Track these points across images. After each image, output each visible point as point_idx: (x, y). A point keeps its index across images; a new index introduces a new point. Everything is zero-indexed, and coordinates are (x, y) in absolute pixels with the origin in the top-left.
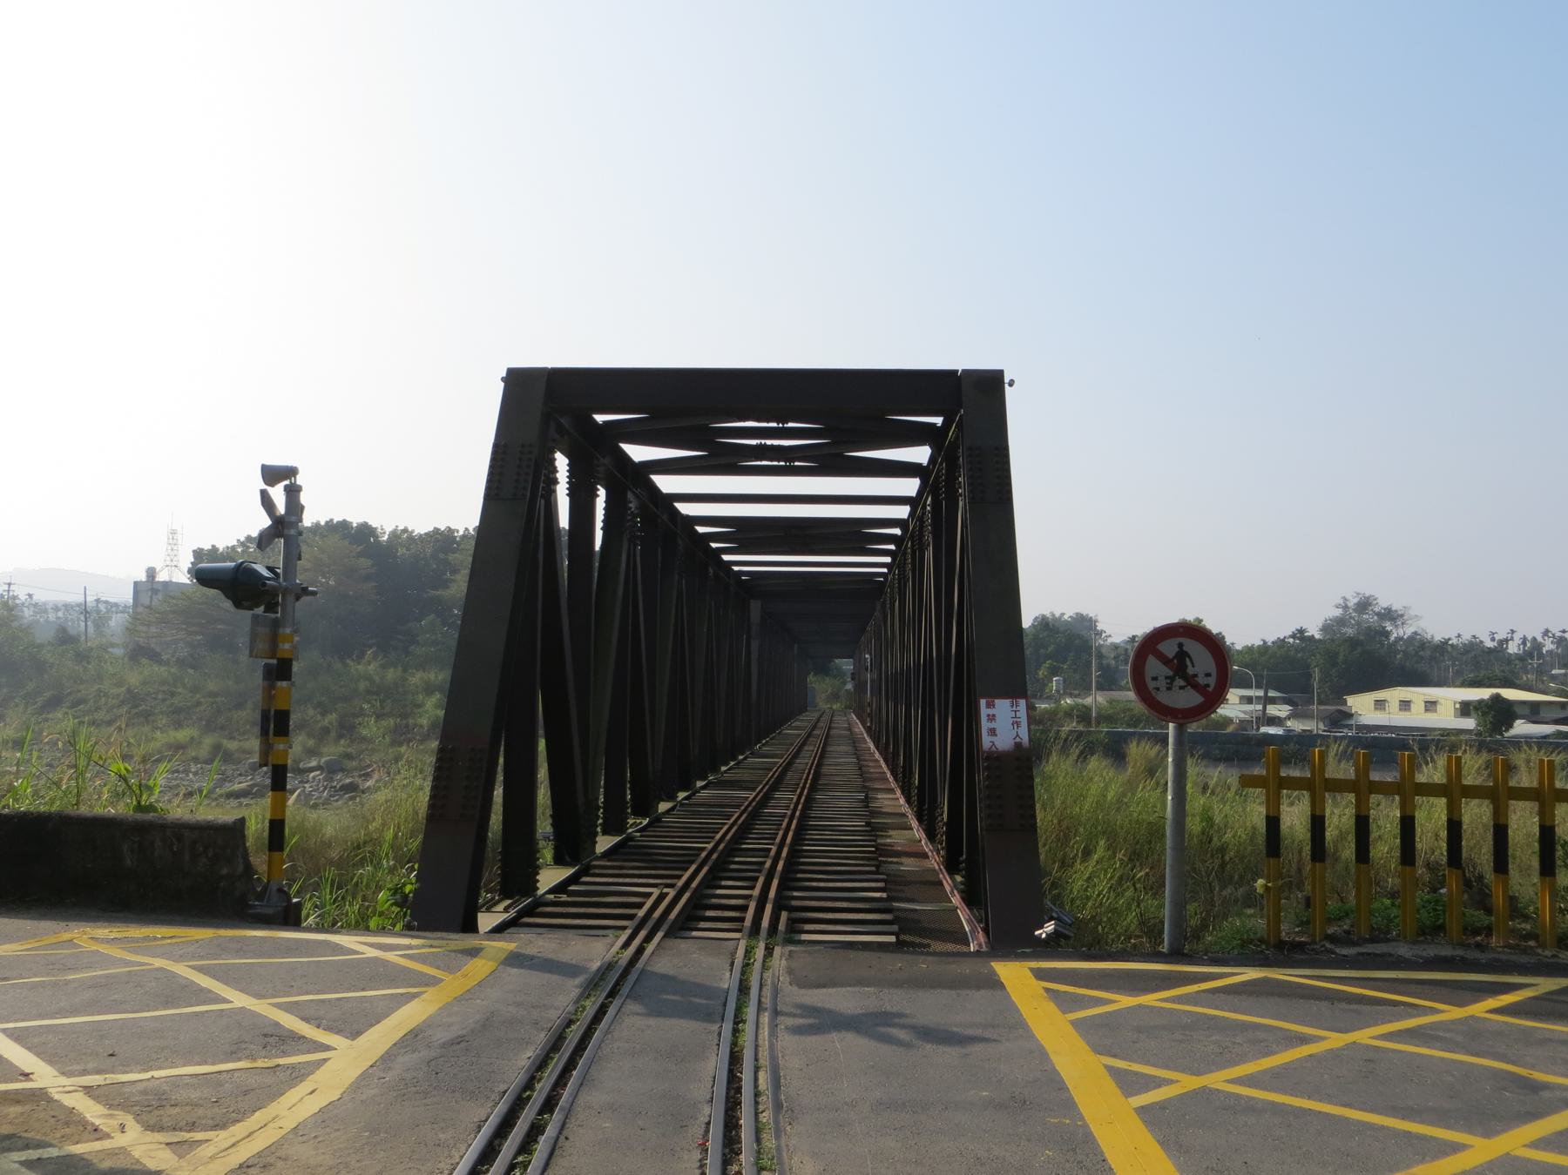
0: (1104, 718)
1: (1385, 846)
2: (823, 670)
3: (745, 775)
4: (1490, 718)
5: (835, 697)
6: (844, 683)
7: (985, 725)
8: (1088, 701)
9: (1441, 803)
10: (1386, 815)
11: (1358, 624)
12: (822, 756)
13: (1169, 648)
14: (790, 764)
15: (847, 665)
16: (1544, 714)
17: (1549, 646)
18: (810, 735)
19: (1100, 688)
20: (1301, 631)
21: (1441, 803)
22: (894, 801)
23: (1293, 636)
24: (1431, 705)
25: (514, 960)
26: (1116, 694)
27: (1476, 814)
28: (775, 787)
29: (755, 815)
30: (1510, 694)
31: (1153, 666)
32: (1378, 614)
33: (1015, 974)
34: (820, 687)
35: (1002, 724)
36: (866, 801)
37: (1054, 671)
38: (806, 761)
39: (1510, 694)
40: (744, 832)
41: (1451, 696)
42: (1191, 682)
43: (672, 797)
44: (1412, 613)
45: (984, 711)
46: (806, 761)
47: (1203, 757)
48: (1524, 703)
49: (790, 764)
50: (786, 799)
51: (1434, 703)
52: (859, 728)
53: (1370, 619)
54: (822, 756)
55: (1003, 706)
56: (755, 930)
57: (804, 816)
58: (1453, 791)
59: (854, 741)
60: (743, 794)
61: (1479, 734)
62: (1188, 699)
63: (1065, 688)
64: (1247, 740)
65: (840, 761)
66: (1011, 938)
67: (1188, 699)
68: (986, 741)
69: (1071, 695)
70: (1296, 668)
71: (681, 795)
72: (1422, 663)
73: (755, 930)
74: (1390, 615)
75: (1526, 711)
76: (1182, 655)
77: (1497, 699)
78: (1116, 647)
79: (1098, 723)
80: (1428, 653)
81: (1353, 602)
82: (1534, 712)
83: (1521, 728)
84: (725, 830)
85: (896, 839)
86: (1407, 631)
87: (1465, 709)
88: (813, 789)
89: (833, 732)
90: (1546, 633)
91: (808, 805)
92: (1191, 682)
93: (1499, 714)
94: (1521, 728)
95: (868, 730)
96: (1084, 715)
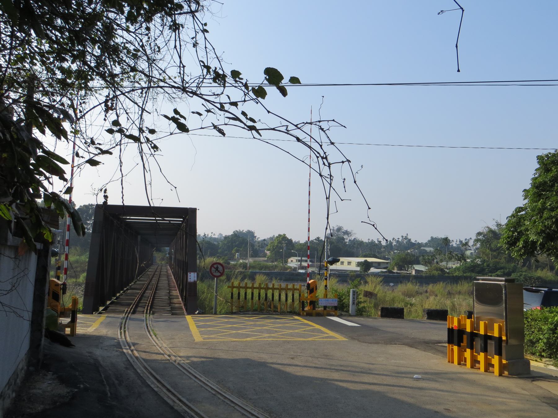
0: (251, 267)
1: (249, 296)
2: (159, 250)
3: (138, 287)
4: (364, 267)
5: (163, 259)
6: (166, 254)
7: (189, 277)
8: (247, 261)
9: (258, 290)
10: (242, 292)
11: (337, 235)
12: (158, 281)
13: (215, 266)
14: (149, 283)
15: (167, 248)
16: (382, 266)
17: (394, 243)
18: (154, 274)
19: (252, 256)
20: (318, 238)
21: (278, 291)
22: (176, 293)
23: (316, 240)
24: (349, 263)
25: (107, 317)
26: (257, 259)
27: (249, 291)
28: (146, 290)
29: (142, 296)
30: (370, 260)
31: (213, 269)
32: (343, 232)
33: (189, 318)
34: (157, 256)
35: (192, 277)
36: (169, 293)
37: (237, 251)
38: (154, 282)
39: (370, 260)
40: (140, 299)
41: (355, 260)
42: (219, 271)
43: (119, 292)
44: (354, 232)
45: (189, 275)
46: (154, 282)
47: (279, 279)
48: (376, 262)
49: (149, 283)
50: (149, 293)
51: (350, 262)
52: (170, 272)
53: (341, 234)
54: (158, 281)
55: (192, 274)
56: (147, 313)
57: (154, 296)
58: (260, 288)
59: (168, 276)
60: (138, 291)
61: (361, 272)
62: (218, 274)
63: (240, 257)
64: (293, 274)
65: (164, 282)
66: (191, 312)
67: (218, 274)
68: (189, 280)
69: (243, 259)
70: (311, 250)
71: (122, 292)
72: (354, 248)
73: (147, 313)
74: (347, 233)
75: (376, 265)
76: (217, 267)
77: (366, 261)
78: (259, 242)
79: (249, 269)
80: (356, 246)
81: (336, 228)
82: (378, 265)
83: (372, 270)
84: (136, 299)
85: (175, 301)
86: (352, 238)
87: (359, 264)
88: (156, 290)
89: (162, 273)
90: (394, 239)
91: (155, 293)
92: (219, 271)
93: (366, 266)
94: (372, 270)
95: (173, 272)
96: (245, 266)
